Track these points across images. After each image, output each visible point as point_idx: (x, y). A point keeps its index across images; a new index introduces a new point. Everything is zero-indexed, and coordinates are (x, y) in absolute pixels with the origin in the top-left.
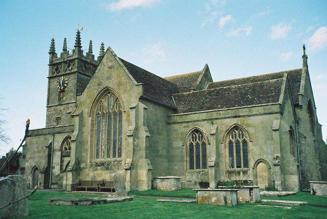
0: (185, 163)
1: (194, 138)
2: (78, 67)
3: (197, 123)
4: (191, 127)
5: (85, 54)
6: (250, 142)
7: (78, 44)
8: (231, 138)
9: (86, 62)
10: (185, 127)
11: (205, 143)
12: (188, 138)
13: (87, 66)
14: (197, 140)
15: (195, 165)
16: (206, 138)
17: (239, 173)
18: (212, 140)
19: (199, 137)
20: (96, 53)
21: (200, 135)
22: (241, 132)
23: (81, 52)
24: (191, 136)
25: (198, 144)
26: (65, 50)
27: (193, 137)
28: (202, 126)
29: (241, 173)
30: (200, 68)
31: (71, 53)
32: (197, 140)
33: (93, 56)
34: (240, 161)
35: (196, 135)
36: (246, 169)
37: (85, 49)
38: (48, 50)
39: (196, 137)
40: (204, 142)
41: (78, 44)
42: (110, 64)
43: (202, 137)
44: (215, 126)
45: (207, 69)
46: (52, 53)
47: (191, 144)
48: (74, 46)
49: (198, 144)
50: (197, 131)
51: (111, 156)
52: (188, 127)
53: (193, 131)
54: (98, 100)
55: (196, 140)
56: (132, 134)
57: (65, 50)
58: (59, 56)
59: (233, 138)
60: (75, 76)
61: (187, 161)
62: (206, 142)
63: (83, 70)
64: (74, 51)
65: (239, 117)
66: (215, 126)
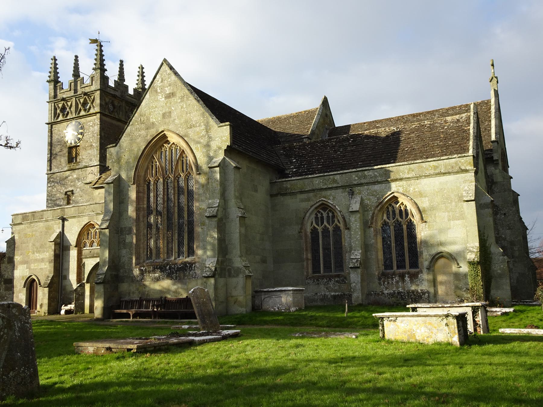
0: (305, 264)
1: (319, 220)
2: (101, 105)
3: (324, 193)
4: (316, 200)
5: (112, 84)
6: (346, 229)
7: (101, 67)
8: (385, 217)
9: (114, 96)
10: (302, 201)
11: (339, 227)
12: (309, 217)
13: (116, 103)
14: (325, 223)
15: (322, 266)
16: (341, 220)
17: (402, 276)
18: (355, 223)
19: (328, 217)
20: (131, 83)
21: (330, 214)
22: (330, 214)
23: (104, 79)
24: (313, 216)
25: (326, 230)
26: (76, 74)
27: (317, 218)
28: (334, 198)
29: (407, 278)
30: (316, 104)
31: (87, 81)
32: (325, 223)
33: (127, 87)
34: (403, 255)
35: (322, 214)
36: (413, 270)
37: (112, 75)
38: (46, 76)
39: (322, 218)
40: (336, 225)
41: (101, 67)
42: (168, 91)
43: (333, 216)
44: (358, 199)
45: (325, 103)
46: (55, 81)
47: (314, 231)
48: (93, 69)
49: (326, 230)
50: (325, 207)
51: (186, 254)
52: (308, 200)
53: (316, 208)
54: (148, 155)
55: (322, 223)
56: (215, 213)
57: (76, 74)
58: (66, 87)
59: (388, 218)
60: (98, 115)
61: (307, 259)
62: (341, 226)
63: (109, 110)
64: (92, 78)
65: (401, 179)
66: (358, 199)
